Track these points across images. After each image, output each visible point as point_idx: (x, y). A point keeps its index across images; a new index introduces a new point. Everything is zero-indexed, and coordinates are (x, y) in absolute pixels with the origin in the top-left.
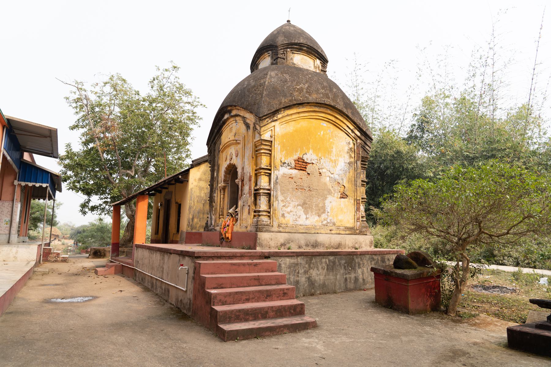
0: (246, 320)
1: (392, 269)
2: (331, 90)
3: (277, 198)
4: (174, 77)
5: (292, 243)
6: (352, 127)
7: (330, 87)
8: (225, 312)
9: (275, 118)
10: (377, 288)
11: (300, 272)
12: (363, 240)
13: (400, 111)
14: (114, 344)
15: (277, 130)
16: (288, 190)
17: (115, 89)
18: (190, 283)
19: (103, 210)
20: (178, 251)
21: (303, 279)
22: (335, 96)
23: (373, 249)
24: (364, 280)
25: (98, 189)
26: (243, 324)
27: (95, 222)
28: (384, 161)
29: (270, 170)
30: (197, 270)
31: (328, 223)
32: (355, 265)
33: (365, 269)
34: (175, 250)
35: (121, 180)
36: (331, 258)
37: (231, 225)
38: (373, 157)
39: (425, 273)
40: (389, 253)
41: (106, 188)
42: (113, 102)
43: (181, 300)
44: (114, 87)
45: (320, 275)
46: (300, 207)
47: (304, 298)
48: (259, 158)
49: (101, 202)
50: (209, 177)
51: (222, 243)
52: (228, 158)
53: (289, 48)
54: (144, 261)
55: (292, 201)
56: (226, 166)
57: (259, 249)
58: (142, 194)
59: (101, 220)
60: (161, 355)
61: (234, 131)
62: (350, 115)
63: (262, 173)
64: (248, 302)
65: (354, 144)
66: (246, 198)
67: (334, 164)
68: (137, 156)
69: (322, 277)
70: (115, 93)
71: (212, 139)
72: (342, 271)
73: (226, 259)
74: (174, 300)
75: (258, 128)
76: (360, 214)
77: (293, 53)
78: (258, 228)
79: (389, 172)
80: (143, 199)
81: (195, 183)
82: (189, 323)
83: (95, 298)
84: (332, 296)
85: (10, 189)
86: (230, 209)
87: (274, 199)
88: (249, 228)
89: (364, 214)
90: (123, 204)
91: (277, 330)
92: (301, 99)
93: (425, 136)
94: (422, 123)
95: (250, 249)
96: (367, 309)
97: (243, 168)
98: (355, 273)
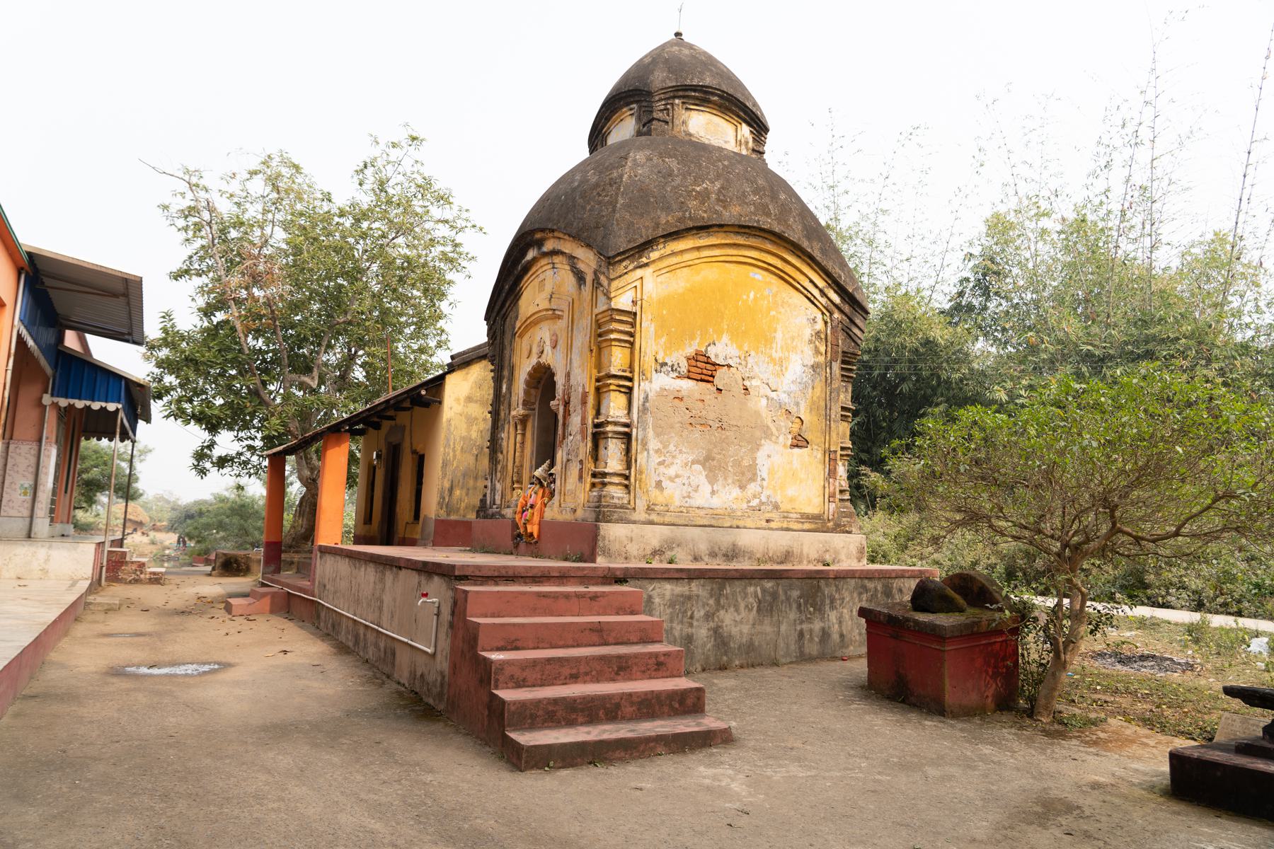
0: (571, 723)
1: (908, 611)
2: (774, 197)
3: (645, 444)
4: (412, 162)
5: (679, 549)
6: (821, 284)
7: (772, 190)
8: (523, 705)
9: (644, 260)
11: (697, 615)
15: (648, 287)
17: (276, 188)
18: (442, 636)
20: (416, 562)
21: (702, 632)
22: (784, 211)
23: (864, 565)
24: (842, 636)
25: (234, 417)
26: (564, 731)
27: (227, 494)
28: (896, 361)
29: (631, 380)
30: (459, 606)
32: (823, 602)
36: (769, 585)
37: (538, 506)
39: (984, 623)
40: (901, 575)
41: (253, 416)
42: (270, 216)
43: (422, 676)
44: (273, 181)
45: (741, 622)
46: (699, 467)
47: (704, 675)
48: (605, 352)
50: (488, 393)
51: (517, 546)
52: (535, 350)
53: (679, 97)
55: (681, 452)
56: (529, 369)
57: (601, 562)
58: (335, 431)
61: (548, 288)
62: (817, 255)
63: (612, 387)
65: (826, 323)
66: (574, 444)
67: (777, 368)
68: (324, 343)
69: (746, 629)
70: (275, 195)
71: (497, 308)
72: (793, 615)
73: (526, 583)
74: (406, 674)
78: (601, 512)
79: (905, 387)
80: (338, 443)
81: (458, 408)
82: (439, 726)
83: (225, 666)
85: (34, 414)
86: (537, 468)
87: (639, 447)
88: (580, 513)
89: (845, 485)
90: (291, 454)
92: (704, 216)
93: (991, 305)
94: (984, 275)
96: (848, 702)
97: (568, 375)
98: (822, 619)
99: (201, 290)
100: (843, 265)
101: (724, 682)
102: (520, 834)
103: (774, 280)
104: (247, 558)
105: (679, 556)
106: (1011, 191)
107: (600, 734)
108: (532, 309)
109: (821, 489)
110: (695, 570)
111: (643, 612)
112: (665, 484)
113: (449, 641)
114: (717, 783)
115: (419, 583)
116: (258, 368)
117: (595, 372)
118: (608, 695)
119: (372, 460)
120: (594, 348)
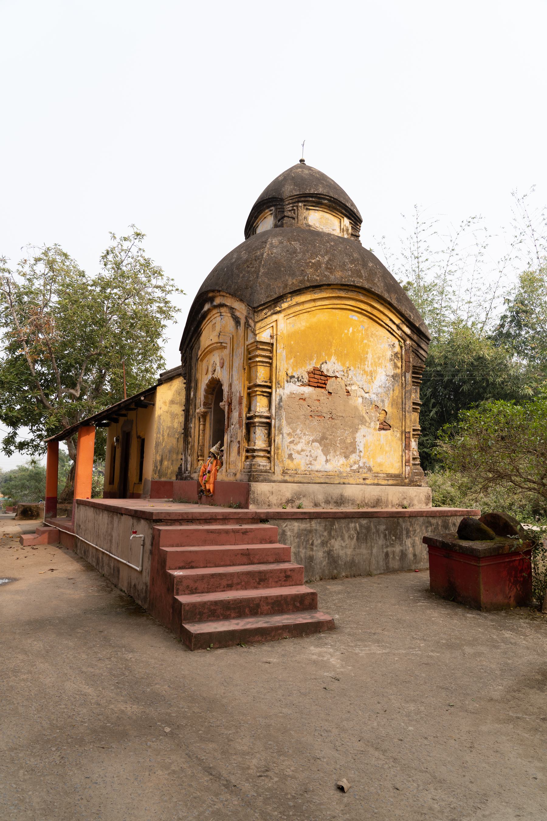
0: (226, 618)
2: (365, 265)
4: (137, 249)
5: (305, 499)
6: (397, 321)
7: (363, 260)
8: (194, 606)
9: (278, 309)
11: (316, 543)
13: (485, 295)
14: (26, 653)
15: (281, 326)
16: (298, 418)
17: (52, 269)
18: (146, 559)
19: (36, 447)
20: (131, 510)
21: (319, 554)
22: (372, 274)
23: (430, 508)
24: (415, 555)
25: (29, 417)
26: (221, 623)
27: (27, 466)
28: (458, 371)
29: (270, 387)
30: (155, 539)
31: (361, 468)
32: (401, 532)
33: (417, 538)
34: (127, 509)
36: (364, 522)
37: (213, 472)
38: (441, 365)
39: (507, 547)
40: (454, 514)
42: (48, 287)
43: (135, 585)
44: (51, 264)
45: (346, 547)
46: (316, 444)
47: (321, 583)
48: (253, 370)
49: (31, 436)
50: (182, 398)
51: (200, 498)
52: (210, 369)
53: (301, 202)
54: (88, 526)
55: (305, 434)
56: (207, 382)
57: (252, 508)
58: (86, 425)
59: (33, 462)
60: (92, 670)
61: (218, 328)
62: (394, 302)
63: (258, 393)
64: (231, 590)
65: (401, 347)
66: (235, 430)
67: (369, 377)
68: (84, 368)
69: (349, 551)
70: (51, 274)
71: (187, 342)
72: (381, 542)
73: (200, 524)
74: (126, 584)
75: (252, 324)
76: (411, 454)
77: (307, 209)
78: (253, 475)
79: (465, 388)
80: (88, 433)
81: (165, 408)
82: (143, 620)
83: (13, 580)
84: (364, 580)
87: (277, 432)
88: (239, 476)
89: (417, 454)
92: (317, 278)
93: (523, 333)
94: (517, 313)
95: (240, 507)
96: (415, 601)
97: (230, 385)
98: (401, 544)
100: (412, 309)
101: (334, 587)
102: (183, 695)
103: (366, 319)
104: (38, 508)
106: (534, 256)
107: (245, 625)
108: (208, 343)
110: (314, 513)
111: (279, 542)
112: (295, 456)
113: (150, 563)
116: (42, 385)
117: (247, 383)
118: (252, 598)
119: (114, 443)
120: (246, 367)
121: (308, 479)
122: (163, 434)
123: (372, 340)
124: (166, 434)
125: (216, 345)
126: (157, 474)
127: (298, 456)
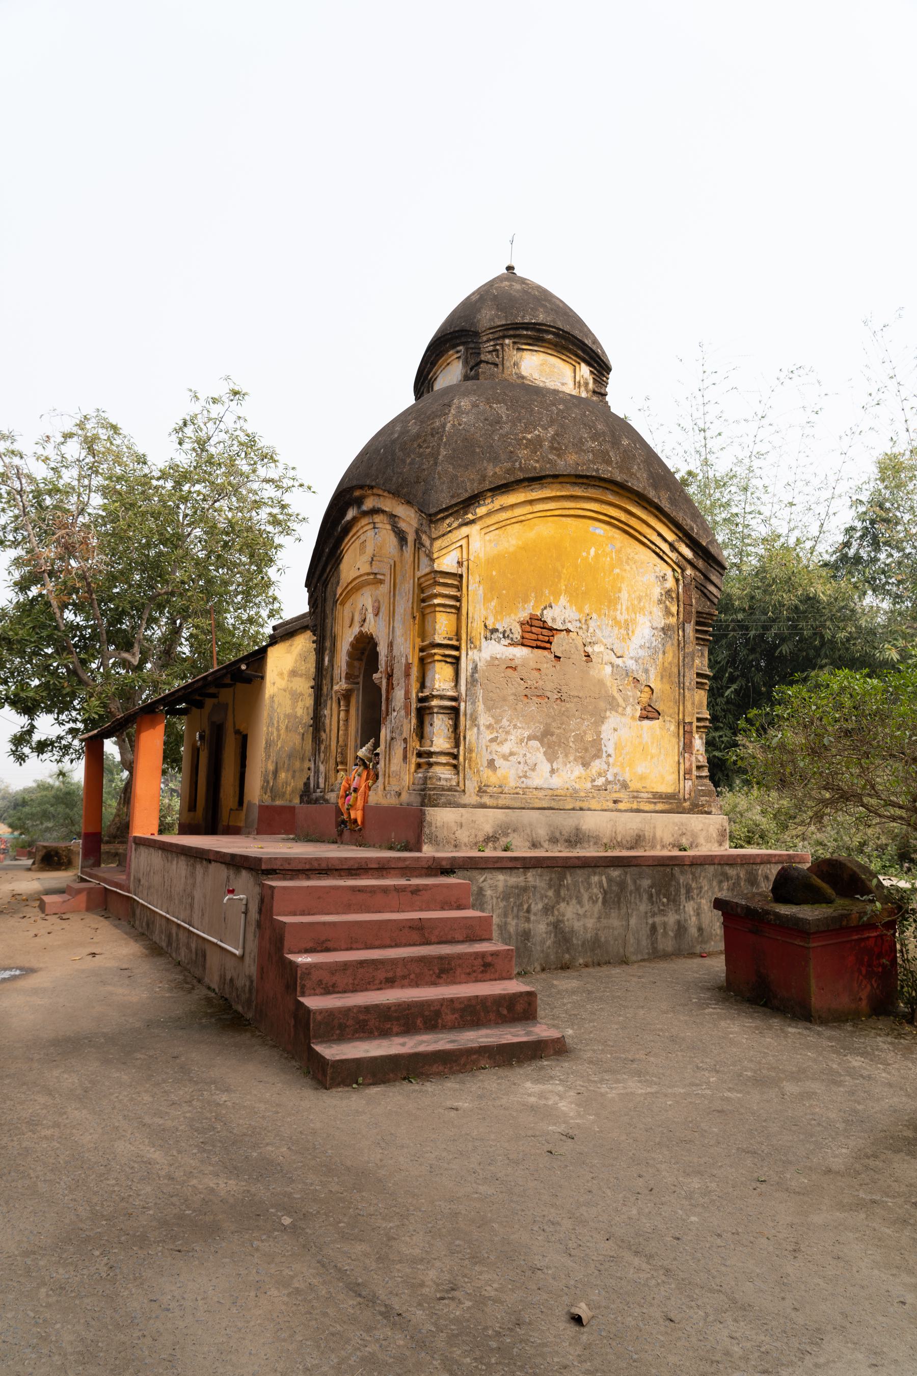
0: (385, 1034)
1: (768, 902)
2: (616, 443)
3: (474, 719)
4: (234, 418)
5: (515, 835)
6: (670, 537)
8: (330, 1014)
10: (730, 952)
11: (534, 908)
12: (700, 826)
13: (817, 493)
14: (50, 1092)
15: (476, 546)
16: (504, 699)
17: (91, 451)
18: (250, 936)
20: (225, 854)
21: (540, 928)
22: (627, 457)
24: (700, 929)
25: (54, 699)
26: (376, 1043)
27: (51, 781)
29: (457, 648)
30: (266, 902)
32: (678, 891)
33: (703, 901)
35: (107, 676)
36: (615, 873)
37: (362, 789)
38: (744, 610)
39: (855, 916)
40: (767, 860)
41: (73, 696)
43: (231, 980)
44: (90, 443)
45: (585, 916)
46: (536, 744)
47: (543, 976)
48: (429, 618)
50: (310, 666)
51: (341, 833)
52: (357, 618)
53: (509, 337)
54: (153, 880)
55: (515, 727)
57: (428, 851)
59: (62, 774)
60: (161, 1122)
61: (369, 550)
62: (665, 505)
63: (437, 657)
64: (392, 987)
65: (677, 580)
66: (398, 720)
67: (623, 631)
68: (145, 616)
69: (590, 923)
70: (90, 459)
71: (318, 573)
72: (643, 907)
73: (341, 877)
74: (216, 978)
75: (427, 542)
76: (693, 759)
77: (519, 349)
78: (428, 795)
79: (785, 649)
80: (153, 724)
81: (282, 683)
82: (245, 1038)
83: (29, 971)
86: (362, 746)
87: (468, 723)
88: (405, 797)
89: (703, 760)
90: (108, 737)
91: (463, 1061)
92: (536, 466)
93: (882, 556)
94: (873, 522)
95: (406, 848)
96: (702, 1005)
97: (391, 645)
98: (677, 911)
99: (17, 562)
100: (696, 515)
101: (565, 983)
104: (69, 850)
105: (514, 843)
107: (416, 1045)
108: (353, 574)
109: (676, 765)
111: (473, 907)
113: (256, 942)
114: (543, 1102)
115: (228, 878)
116: (76, 646)
117: (418, 641)
118: (427, 1001)
119: (195, 741)
120: (417, 615)
121: (520, 802)
122: (278, 726)
123: (628, 568)
124: (284, 727)
125: (366, 577)
126: (269, 794)
127: (505, 763)
